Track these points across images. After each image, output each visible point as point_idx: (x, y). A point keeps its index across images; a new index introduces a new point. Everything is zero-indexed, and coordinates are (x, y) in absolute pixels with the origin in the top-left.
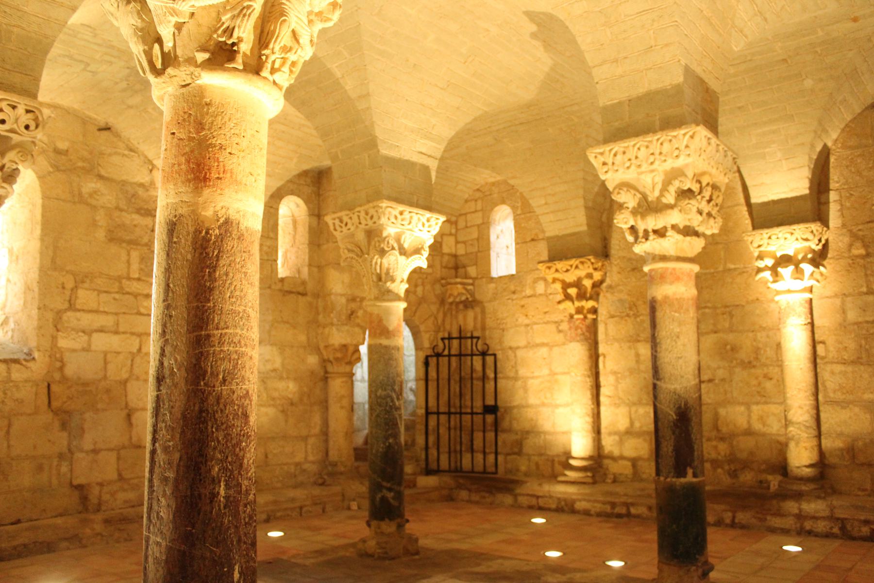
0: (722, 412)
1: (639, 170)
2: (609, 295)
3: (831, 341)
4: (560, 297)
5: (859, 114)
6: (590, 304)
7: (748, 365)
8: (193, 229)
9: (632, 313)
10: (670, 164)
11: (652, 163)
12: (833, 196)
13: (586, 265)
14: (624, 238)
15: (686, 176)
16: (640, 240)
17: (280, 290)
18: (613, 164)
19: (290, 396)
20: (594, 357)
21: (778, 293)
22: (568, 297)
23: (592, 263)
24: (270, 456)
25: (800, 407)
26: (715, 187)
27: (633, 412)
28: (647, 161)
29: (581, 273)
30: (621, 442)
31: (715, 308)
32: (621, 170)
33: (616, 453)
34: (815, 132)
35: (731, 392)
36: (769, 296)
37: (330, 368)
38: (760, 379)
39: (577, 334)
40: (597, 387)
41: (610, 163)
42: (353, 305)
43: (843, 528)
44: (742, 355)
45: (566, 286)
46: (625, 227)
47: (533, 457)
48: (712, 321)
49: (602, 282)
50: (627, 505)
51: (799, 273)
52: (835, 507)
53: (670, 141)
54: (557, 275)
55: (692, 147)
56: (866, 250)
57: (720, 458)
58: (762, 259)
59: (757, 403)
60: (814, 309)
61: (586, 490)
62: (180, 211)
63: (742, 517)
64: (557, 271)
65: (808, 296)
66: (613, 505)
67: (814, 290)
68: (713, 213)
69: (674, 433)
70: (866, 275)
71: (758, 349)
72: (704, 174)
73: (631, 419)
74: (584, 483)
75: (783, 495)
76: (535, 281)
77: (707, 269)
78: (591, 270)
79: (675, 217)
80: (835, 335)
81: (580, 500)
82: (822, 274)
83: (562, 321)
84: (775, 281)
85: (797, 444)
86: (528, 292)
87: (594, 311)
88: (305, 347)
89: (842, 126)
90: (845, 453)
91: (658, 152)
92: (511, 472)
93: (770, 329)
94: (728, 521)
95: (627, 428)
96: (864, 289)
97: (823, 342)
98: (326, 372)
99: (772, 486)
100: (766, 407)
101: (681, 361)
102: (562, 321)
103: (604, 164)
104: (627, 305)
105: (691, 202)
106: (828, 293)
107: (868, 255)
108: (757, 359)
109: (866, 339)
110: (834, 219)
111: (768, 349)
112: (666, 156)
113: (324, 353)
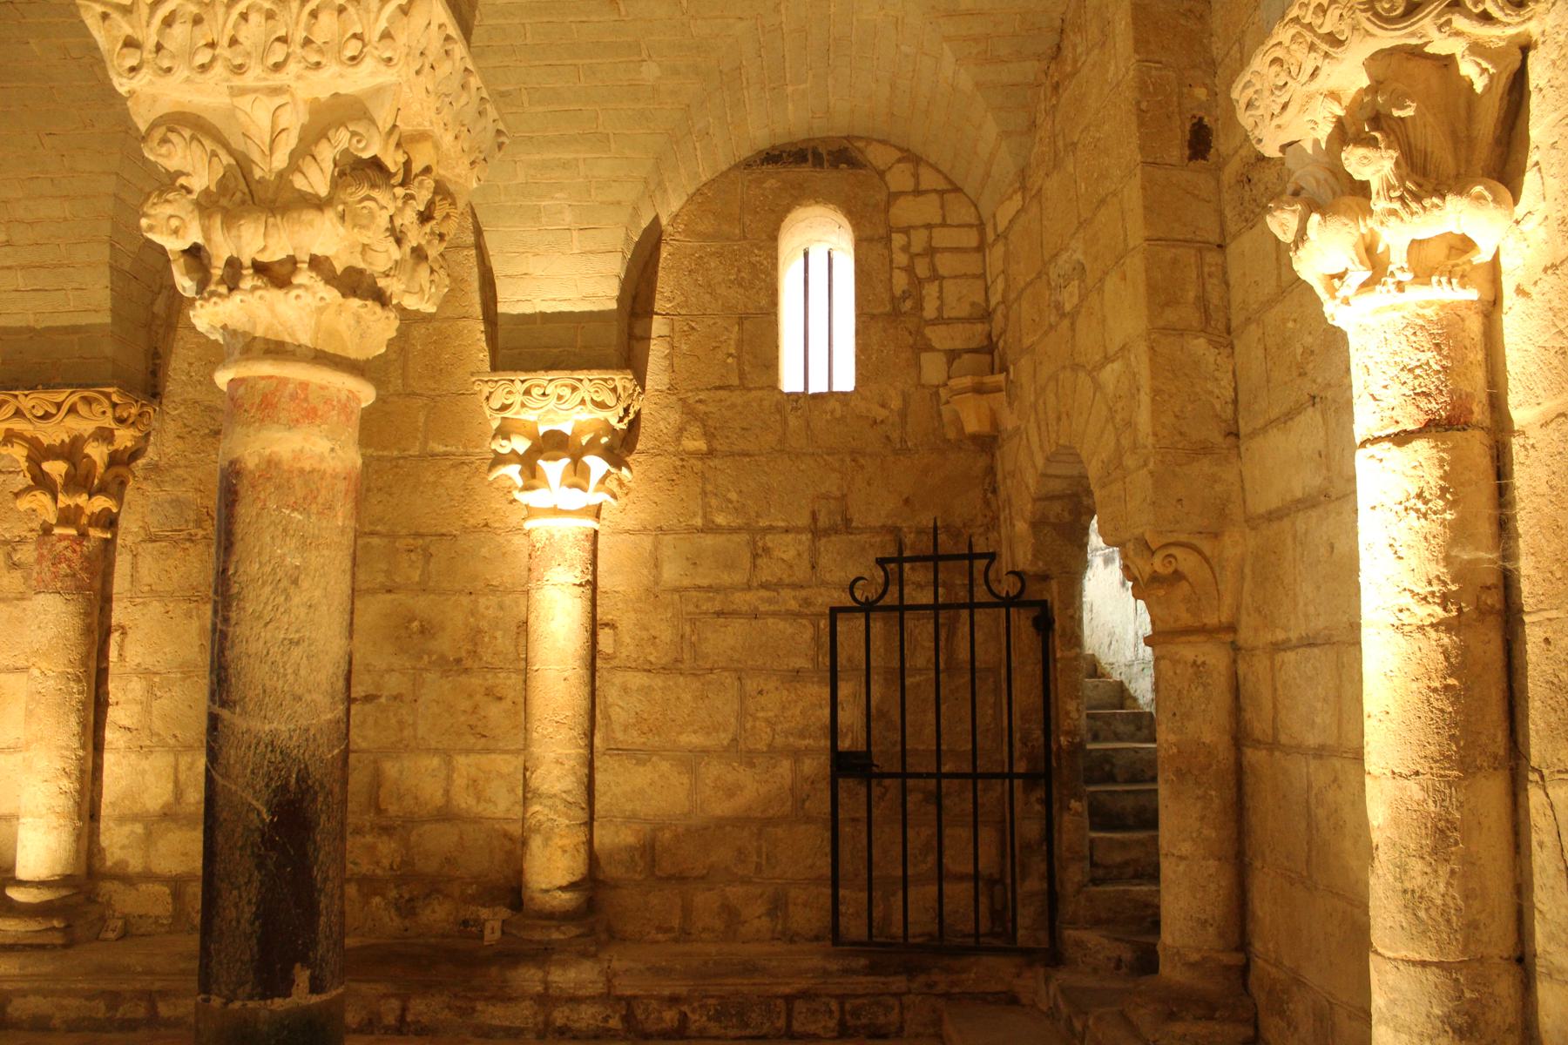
0: (390, 768)
1: (237, 81)
2: (148, 487)
3: (626, 622)
4: (24, 480)
5: (724, 174)
6: (100, 503)
7: (454, 666)
9: (201, 533)
10: (333, 81)
11: (277, 67)
12: (658, 326)
13: (96, 408)
15: (373, 122)
16: (212, 287)
18: (159, 47)
20: (97, 634)
21: (531, 512)
22: (41, 482)
23: (115, 405)
25: (558, 762)
26: (441, 190)
27: (183, 767)
29: (84, 425)
30: (149, 838)
31: (392, 536)
32: (181, 73)
33: (135, 864)
34: (646, 181)
35: (414, 725)
36: (513, 520)
38: (478, 697)
39: (56, 576)
40: (97, 706)
41: (150, 44)
43: (628, 1018)
44: (443, 644)
45: (39, 453)
46: (174, 245)
49: (135, 454)
50: (150, 997)
51: (578, 472)
52: (615, 975)
54: (18, 425)
55: (402, 39)
56: (709, 443)
57: (379, 872)
58: (507, 437)
59: (468, 751)
60: (600, 554)
61: (43, 966)
63: (422, 1008)
65: (591, 524)
66: (114, 998)
67: (603, 514)
68: (433, 252)
69: (260, 866)
70: (704, 493)
71: (479, 631)
72: (421, 137)
73: (176, 782)
74: (41, 947)
75: (512, 955)
77: (385, 448)
78: (108, 422)
79: (324, 236)
80: (635, 611)
81: (24, 994)
82: (621, 483)
83: (22, 541)
84: (526, 488)
85: (547, 840)
87: (109, 521)
89: (691, 190)
90: (637, 857)
91: (300, 35)
93: (508, 592)
94: (390, 1019)
95: (166, 805)
96: (699, 522)
97: (611, 625)
99: (487, 932)
100: (484, 760)
101: (297, 652)
102: (22, 541)
103: (130, 43)
104: (192, 516)
105: (375, 193)
106: (629, 523)
107: (711, 453)
108: (474, 653)
109: (693, 622)
110: (656, 375)
111: (499, 634)
112: (320, 51)
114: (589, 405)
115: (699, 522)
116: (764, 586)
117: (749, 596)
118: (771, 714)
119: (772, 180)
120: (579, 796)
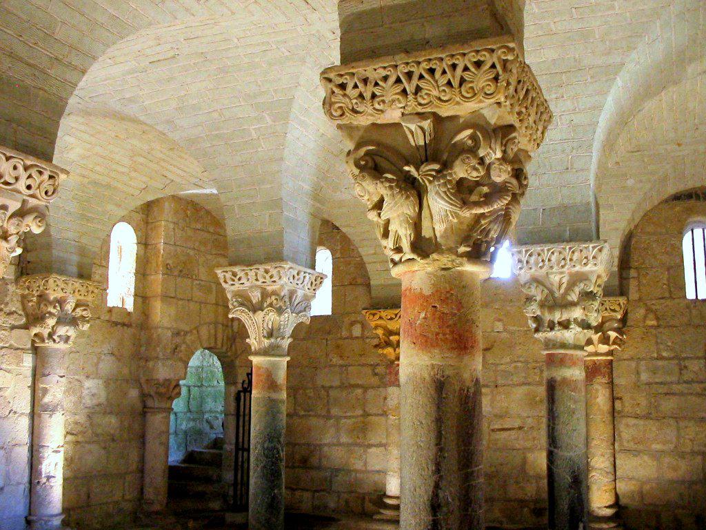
5: (656, 207)
8: (458, 388)
11: (563, 267)
14: (527, 323)
17: (108, 321)
19: (112, 432)
24: (92, 496)
28: (558, 265)
37: (150, 403)
42: (178, 340)
47: (343, 495)
48: (524, 375)
53: (581, 251)
62: (447, 373)
64: (381, 318)
70: (657, 343)
76: (353, 324)
79: (577, 313)
83: (378, 365)
86: (345, 333)
88: (127, 381)
92: (319, 508)
96: (655, 355)
98: (145, 407)
102: (378, 365)
105: (593, 303)
107: (659, 326)
113: (144, 386)
114: (609, 311)
115: (655, 355)
116: (685, 382)
117: (679, 387)
118: (691, 437)
119: (679, 207)
120: (611, 469)
